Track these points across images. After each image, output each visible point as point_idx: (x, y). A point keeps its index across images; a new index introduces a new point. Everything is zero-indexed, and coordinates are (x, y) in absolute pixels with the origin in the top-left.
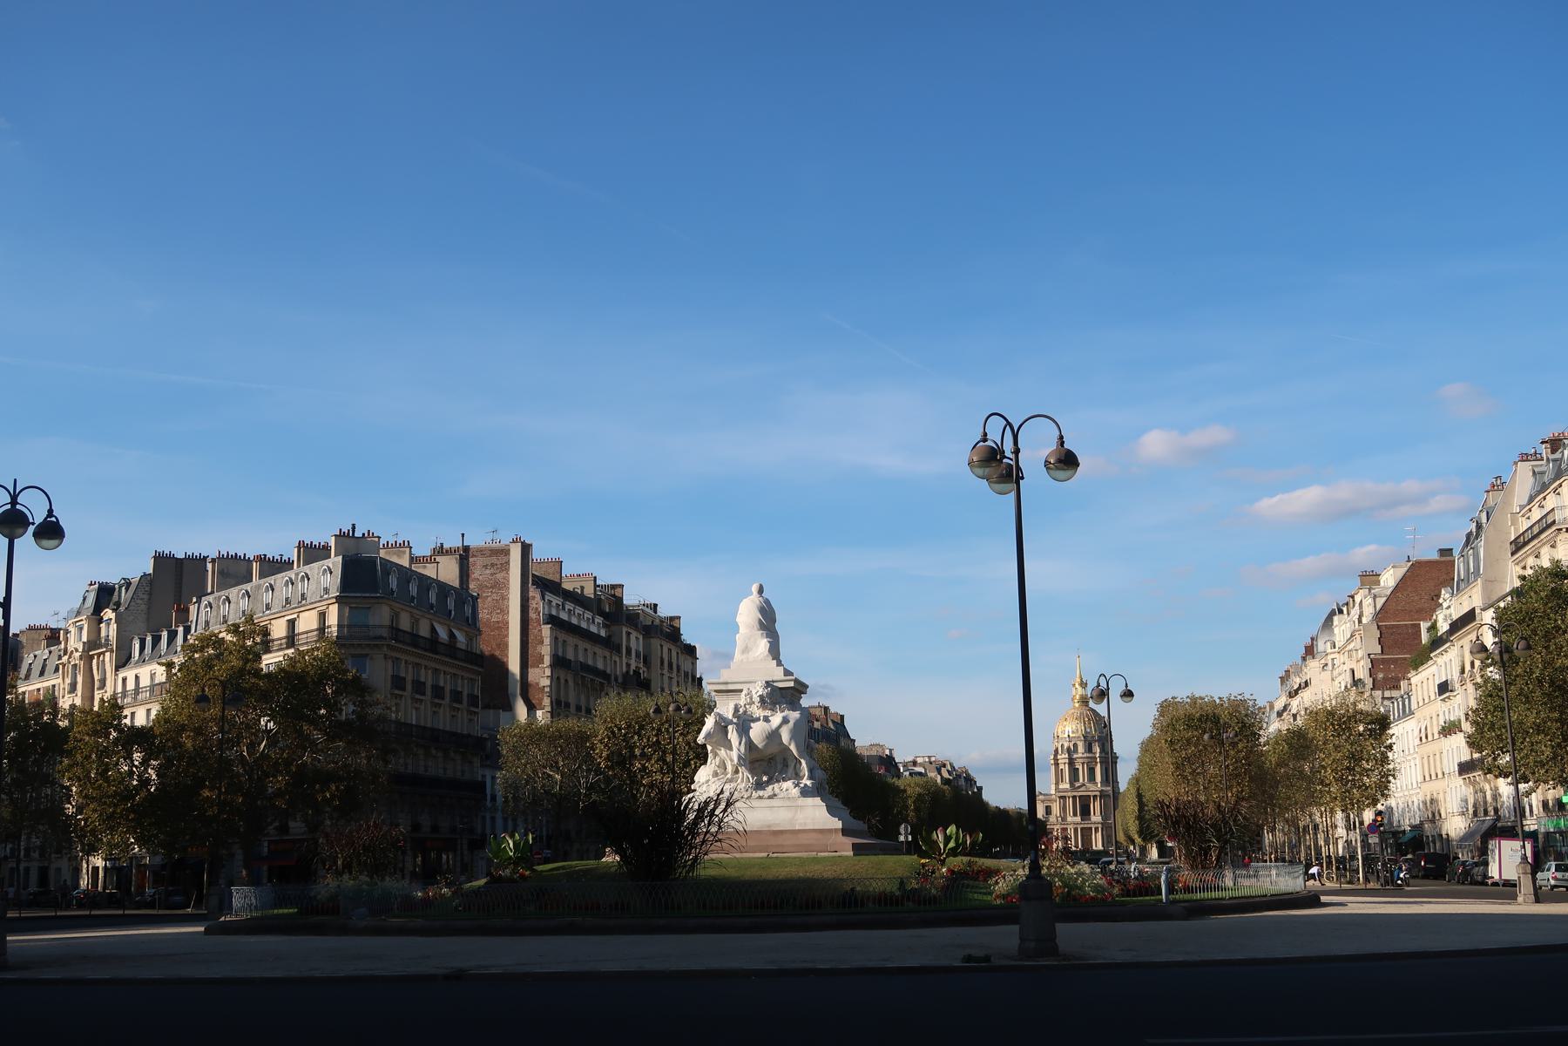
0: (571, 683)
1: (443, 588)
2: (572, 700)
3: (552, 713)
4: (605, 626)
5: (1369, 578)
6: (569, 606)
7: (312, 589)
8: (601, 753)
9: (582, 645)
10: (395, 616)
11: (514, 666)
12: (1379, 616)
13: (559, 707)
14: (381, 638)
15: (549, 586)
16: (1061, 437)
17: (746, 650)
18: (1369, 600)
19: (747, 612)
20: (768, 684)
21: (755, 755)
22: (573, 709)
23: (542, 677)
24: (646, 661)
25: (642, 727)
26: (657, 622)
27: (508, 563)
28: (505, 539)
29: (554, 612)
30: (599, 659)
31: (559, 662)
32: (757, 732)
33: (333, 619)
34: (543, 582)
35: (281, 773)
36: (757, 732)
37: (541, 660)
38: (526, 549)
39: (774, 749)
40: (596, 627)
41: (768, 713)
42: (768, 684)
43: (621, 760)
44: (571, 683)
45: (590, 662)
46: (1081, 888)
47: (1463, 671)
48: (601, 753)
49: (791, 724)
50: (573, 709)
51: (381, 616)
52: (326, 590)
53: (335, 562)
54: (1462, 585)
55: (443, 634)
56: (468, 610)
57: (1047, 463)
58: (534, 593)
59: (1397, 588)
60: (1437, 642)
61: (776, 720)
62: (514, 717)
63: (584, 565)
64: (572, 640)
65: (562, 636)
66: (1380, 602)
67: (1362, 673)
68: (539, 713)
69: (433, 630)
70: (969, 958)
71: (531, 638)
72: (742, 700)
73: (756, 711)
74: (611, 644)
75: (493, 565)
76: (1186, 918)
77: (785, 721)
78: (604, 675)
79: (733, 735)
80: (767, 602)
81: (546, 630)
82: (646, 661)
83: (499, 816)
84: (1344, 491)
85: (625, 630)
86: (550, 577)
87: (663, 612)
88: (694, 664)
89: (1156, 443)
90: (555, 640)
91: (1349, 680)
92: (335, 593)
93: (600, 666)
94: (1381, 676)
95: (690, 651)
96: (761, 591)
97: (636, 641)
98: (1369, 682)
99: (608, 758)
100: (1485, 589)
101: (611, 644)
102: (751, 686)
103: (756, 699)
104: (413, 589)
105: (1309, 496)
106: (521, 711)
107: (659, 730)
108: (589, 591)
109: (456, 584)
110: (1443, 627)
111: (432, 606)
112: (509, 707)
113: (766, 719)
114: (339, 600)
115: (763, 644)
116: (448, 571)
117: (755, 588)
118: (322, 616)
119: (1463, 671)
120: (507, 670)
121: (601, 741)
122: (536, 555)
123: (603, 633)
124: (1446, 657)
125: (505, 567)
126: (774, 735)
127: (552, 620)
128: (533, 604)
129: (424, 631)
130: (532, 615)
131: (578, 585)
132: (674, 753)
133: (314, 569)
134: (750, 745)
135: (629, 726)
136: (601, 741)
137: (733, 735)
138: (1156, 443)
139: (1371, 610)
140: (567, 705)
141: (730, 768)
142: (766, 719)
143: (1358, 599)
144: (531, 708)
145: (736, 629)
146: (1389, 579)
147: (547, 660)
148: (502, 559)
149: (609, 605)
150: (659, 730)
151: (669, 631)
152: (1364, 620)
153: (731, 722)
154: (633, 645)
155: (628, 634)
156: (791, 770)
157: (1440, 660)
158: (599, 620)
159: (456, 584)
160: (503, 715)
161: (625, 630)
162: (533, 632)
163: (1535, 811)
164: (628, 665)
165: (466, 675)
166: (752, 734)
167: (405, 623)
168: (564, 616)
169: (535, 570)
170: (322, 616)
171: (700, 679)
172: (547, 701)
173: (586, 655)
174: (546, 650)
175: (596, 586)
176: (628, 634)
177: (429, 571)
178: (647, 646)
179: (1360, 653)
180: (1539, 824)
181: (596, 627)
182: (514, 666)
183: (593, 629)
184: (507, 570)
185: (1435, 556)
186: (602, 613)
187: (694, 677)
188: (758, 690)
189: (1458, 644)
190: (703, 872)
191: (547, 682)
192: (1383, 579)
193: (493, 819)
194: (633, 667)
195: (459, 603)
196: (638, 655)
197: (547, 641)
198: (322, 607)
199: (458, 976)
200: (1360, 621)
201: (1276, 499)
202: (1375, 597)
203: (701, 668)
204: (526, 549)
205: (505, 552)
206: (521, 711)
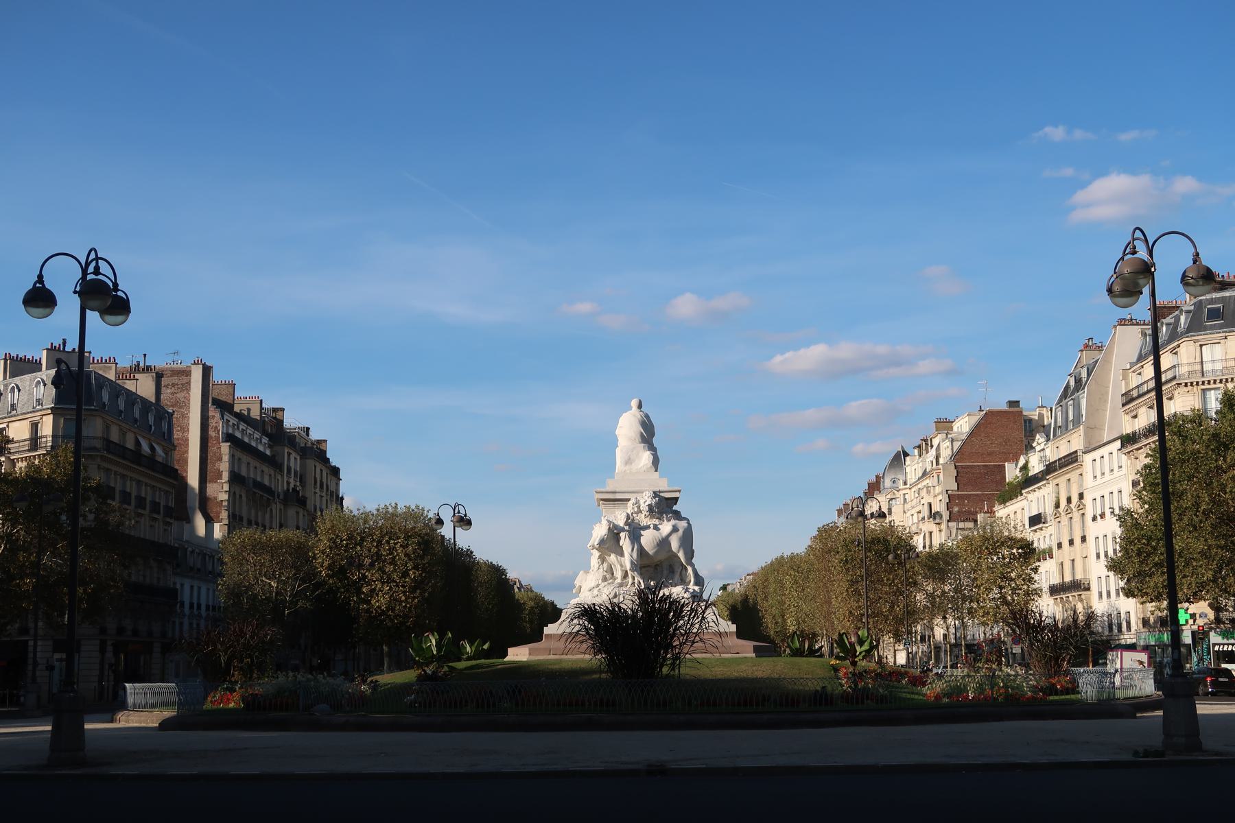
0: (244, 498)
1: (132, 398)
2: (244, 514)
3: (229, 525)
4: (270, 447)
5: (944, 425)
6: (243, 426)
7: (23, 401)
8: (322, 564)
9: (254, 463)
10: (107, 428)
11: (193, 480)
12: (957, 457)
13: (235, 522)
14: (95, 449)
15: (225, 407)
16: (1198, 254)
17: (628, 461)
18: (948, 443)
19: (627, 426)
20: (656, 494)
21: (646, 562)
22: (245, 522)
23: (220, 491)
24: (302, 481)
25: (363, 539)
26: (309, 444)
27: (189, 383)
28: (185, 361)
29: (230, 431)
30: (266, 476)
31: (235, 478)
32: (648, 539)
33: (47, 428)
34: (219, 403)
35: (27, 576)
36: (648, 539)
37: (220, 475)
38: (207, 371)
39: (662, 556)
40: (263, 446)
41: (657, 522)
42: (656, 494)
43: (340, 572)
44: (244, 498)
45: (259, 479)
46: (1019, 687)
47: (1057, 506)
48: (322, 564)
49: (681, 532)
50: (245, 522)
51: (94, 428)
52: (39, 402)
53: (47, 374)
54: (1059, 432)
55: (145, 447)
56: (164, 426)
57: (1184, 276)
58: (214, 412)
59: (972, 434)
60: (1029, 481)
61: (666, 527)
62: (193, 529)
63: (255, 390)
64: (245, 458)
65: (238, 454)
66: (957, 445)
67: (940, 506)
68: (217, 526)
69: (138, 443)
70: (1136, 753)
71: (210, 454)
72: (630, 508)
73: (643, 519)
74: (274, 463)
75: (173, 385)
76: (205, 729)
77: (675, 529)
78: (269, 490)
79: (625, 542)
80: (647, 416)
81: (225, 448)
82: (302, 481)
83: (186, 621)
84: (846, 350)
85: (286, 450)
86: (223, 398)
87: (314, 436)
88: (338, 484)
89: (686, 306)
90: (232, 456)
91: (926, 513)
92: (49, 404)
93: (266, 482)
94: (956, 509)
95: (335, 471)
96: (640, 406)
97: (293, 461)
98: (946, 515)
99: (329, 568)
100: (1086, 434)
101: (274, 463)
102: (639, 496)
103: (644, 507)
104: (121, 404)
105: (817, 352)
106: (200, 524)
107: (379, 542)
108: (255, 413)
109: (153, 400)
110: (1036, 467)
111: (136, 420)
112: (189, 520)
113: (656, 528)
114: (54, 411)
115: (646, 457)
116: (144, 387)
117: (634, 403)
118: (35, 426)
119: (1057, 506)
120: (186, 484)
121: (323, 552)
122: (216, 377)
123: (268, 452)
124: (1038, 494)
125: (187, 387)
126: (664, 543)
127: (229, 438)
128: (212, 423)
129: (130, 444)
130: (212, 433)
131: (244, 407)
132: (393, 562)
133: (25, 381)
134: (642, 551)
135: (350, 538)
136: (323, 552)
137: (625, 542)
138: (686, 306)
139: (949, 452)
140: (241, 519)
141: (618, 574)
142: (656, 528)
143: (935, 442)
144: (209, 521)
145: (615, 443)
146: (963, 426)
147: (226, 476)
148: (184, 380)
149: (271, 425)
150: (379, 542)
151: (317, 452)
152: (941, 461)
153: (623, 530)
154: (292, 465)
155: (289, 454)
156: (677, 577)
157: (1030, 496)
158: (265, 440)
159: (153, 400)
160: (186, 526)
161: (286, 450)
162: (212, 449)
163: (1134, 626)
164: (288, 483)
165: (164, 487)
166: (643, 541)
167: (115, 436)
168: (238, 435)
169: (214, 393)
170: (35, 426)
171: (342, 499)
172: (224, 515)
173: (262, 477)
174: (224, 467)
175: (262, 408)
176: (289, 454)
177: (130, 385)
178: (303, 466)
179: (938, 489)
180: (1139, 638)
181: (263, 446)
182: (193, 480)
183: (261, 448)
184: (188, 390)
185: (1004, 407)
186: (265, 433)
187: (337, 496)
188: (646, 500)
189: (1053, 483)
190: (686, 671)
191: (224, 497)
192: (956, 427)
193: (181, 624)
194: (292, 486)
195: (158, 420)
196: (296, 475)
197: (226, 458)
198: (35, 417)
199: (657, 771)
200: (937, 463)
201: (787, 355)
202: (952, 441)
203: (344, 489)
204: (207, 371)
205: (187, 373)
206: (200, 524)
